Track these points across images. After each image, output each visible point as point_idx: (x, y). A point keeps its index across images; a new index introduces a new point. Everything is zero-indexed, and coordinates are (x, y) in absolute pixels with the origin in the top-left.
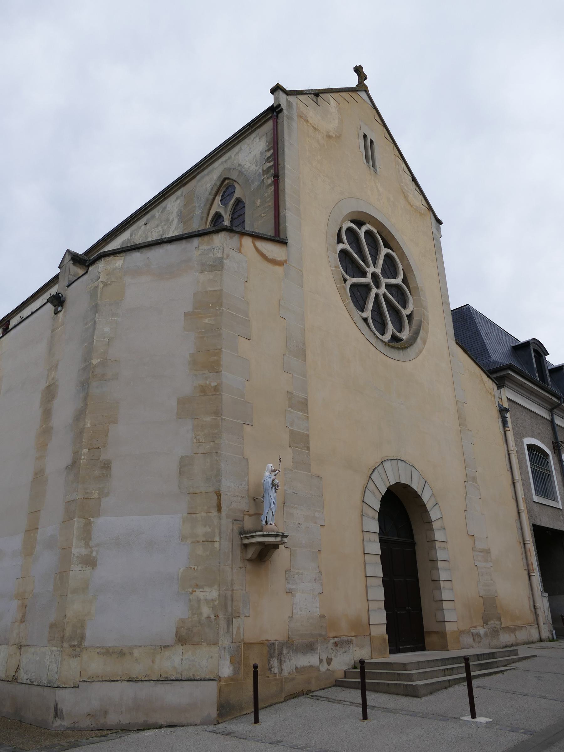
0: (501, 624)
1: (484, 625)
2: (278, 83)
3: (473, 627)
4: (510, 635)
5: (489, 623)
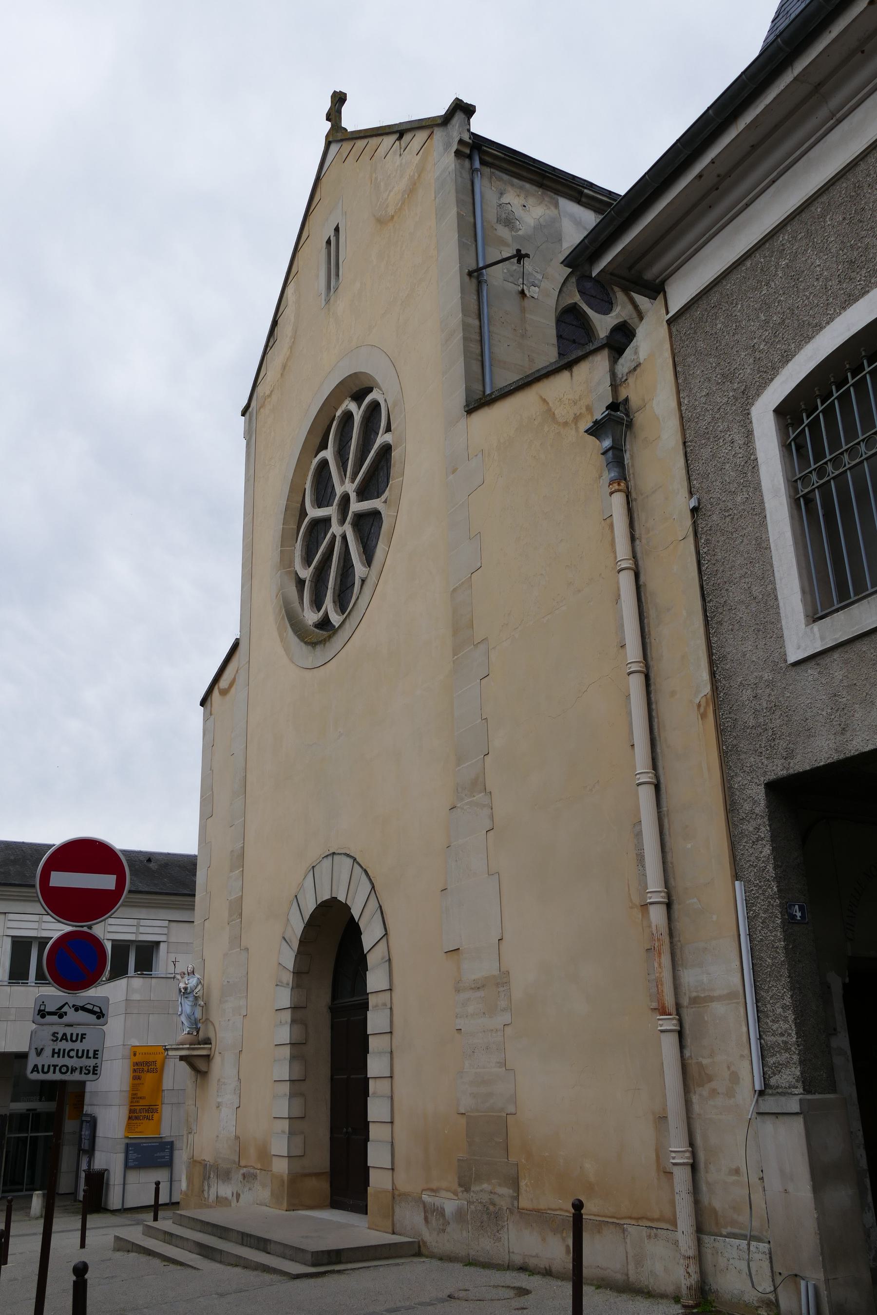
0: (517, 1198)
1: (460, 1189)
2: (457, 99)
3: (428, 1189)
4: (544, 1240)
5: (475, 1188)
